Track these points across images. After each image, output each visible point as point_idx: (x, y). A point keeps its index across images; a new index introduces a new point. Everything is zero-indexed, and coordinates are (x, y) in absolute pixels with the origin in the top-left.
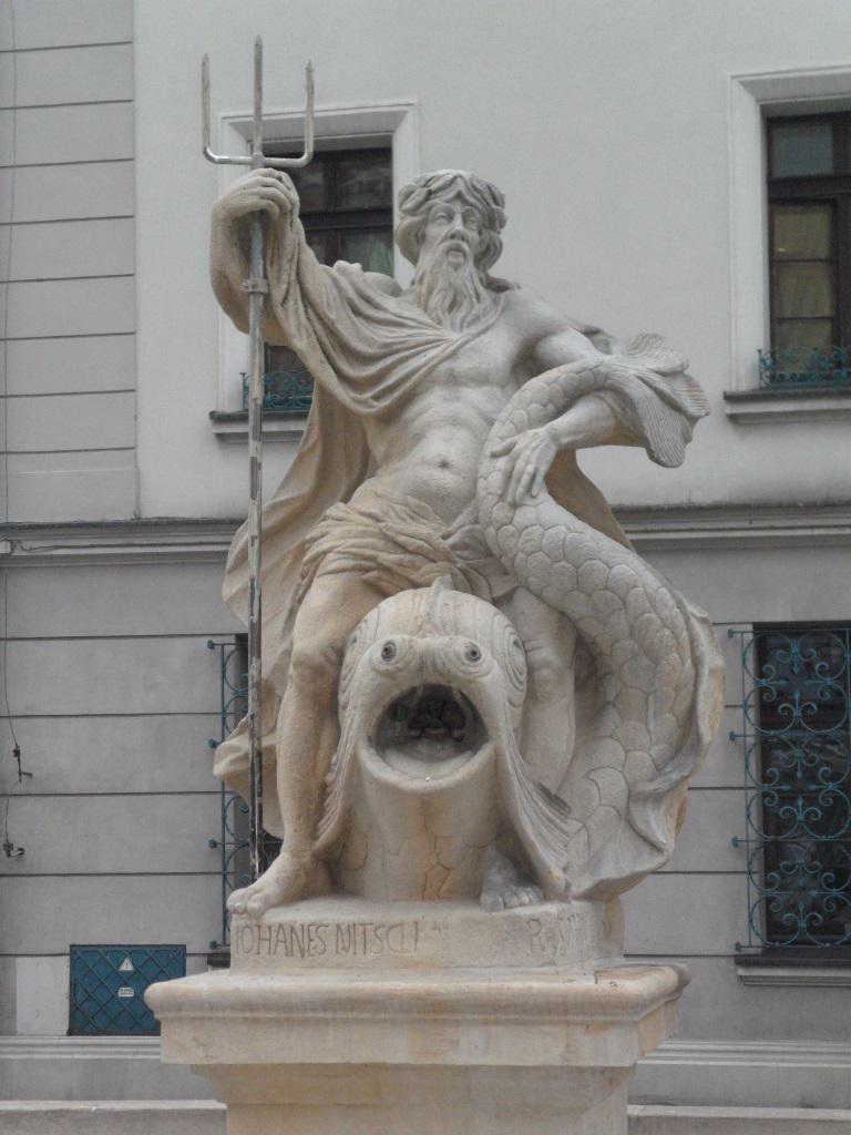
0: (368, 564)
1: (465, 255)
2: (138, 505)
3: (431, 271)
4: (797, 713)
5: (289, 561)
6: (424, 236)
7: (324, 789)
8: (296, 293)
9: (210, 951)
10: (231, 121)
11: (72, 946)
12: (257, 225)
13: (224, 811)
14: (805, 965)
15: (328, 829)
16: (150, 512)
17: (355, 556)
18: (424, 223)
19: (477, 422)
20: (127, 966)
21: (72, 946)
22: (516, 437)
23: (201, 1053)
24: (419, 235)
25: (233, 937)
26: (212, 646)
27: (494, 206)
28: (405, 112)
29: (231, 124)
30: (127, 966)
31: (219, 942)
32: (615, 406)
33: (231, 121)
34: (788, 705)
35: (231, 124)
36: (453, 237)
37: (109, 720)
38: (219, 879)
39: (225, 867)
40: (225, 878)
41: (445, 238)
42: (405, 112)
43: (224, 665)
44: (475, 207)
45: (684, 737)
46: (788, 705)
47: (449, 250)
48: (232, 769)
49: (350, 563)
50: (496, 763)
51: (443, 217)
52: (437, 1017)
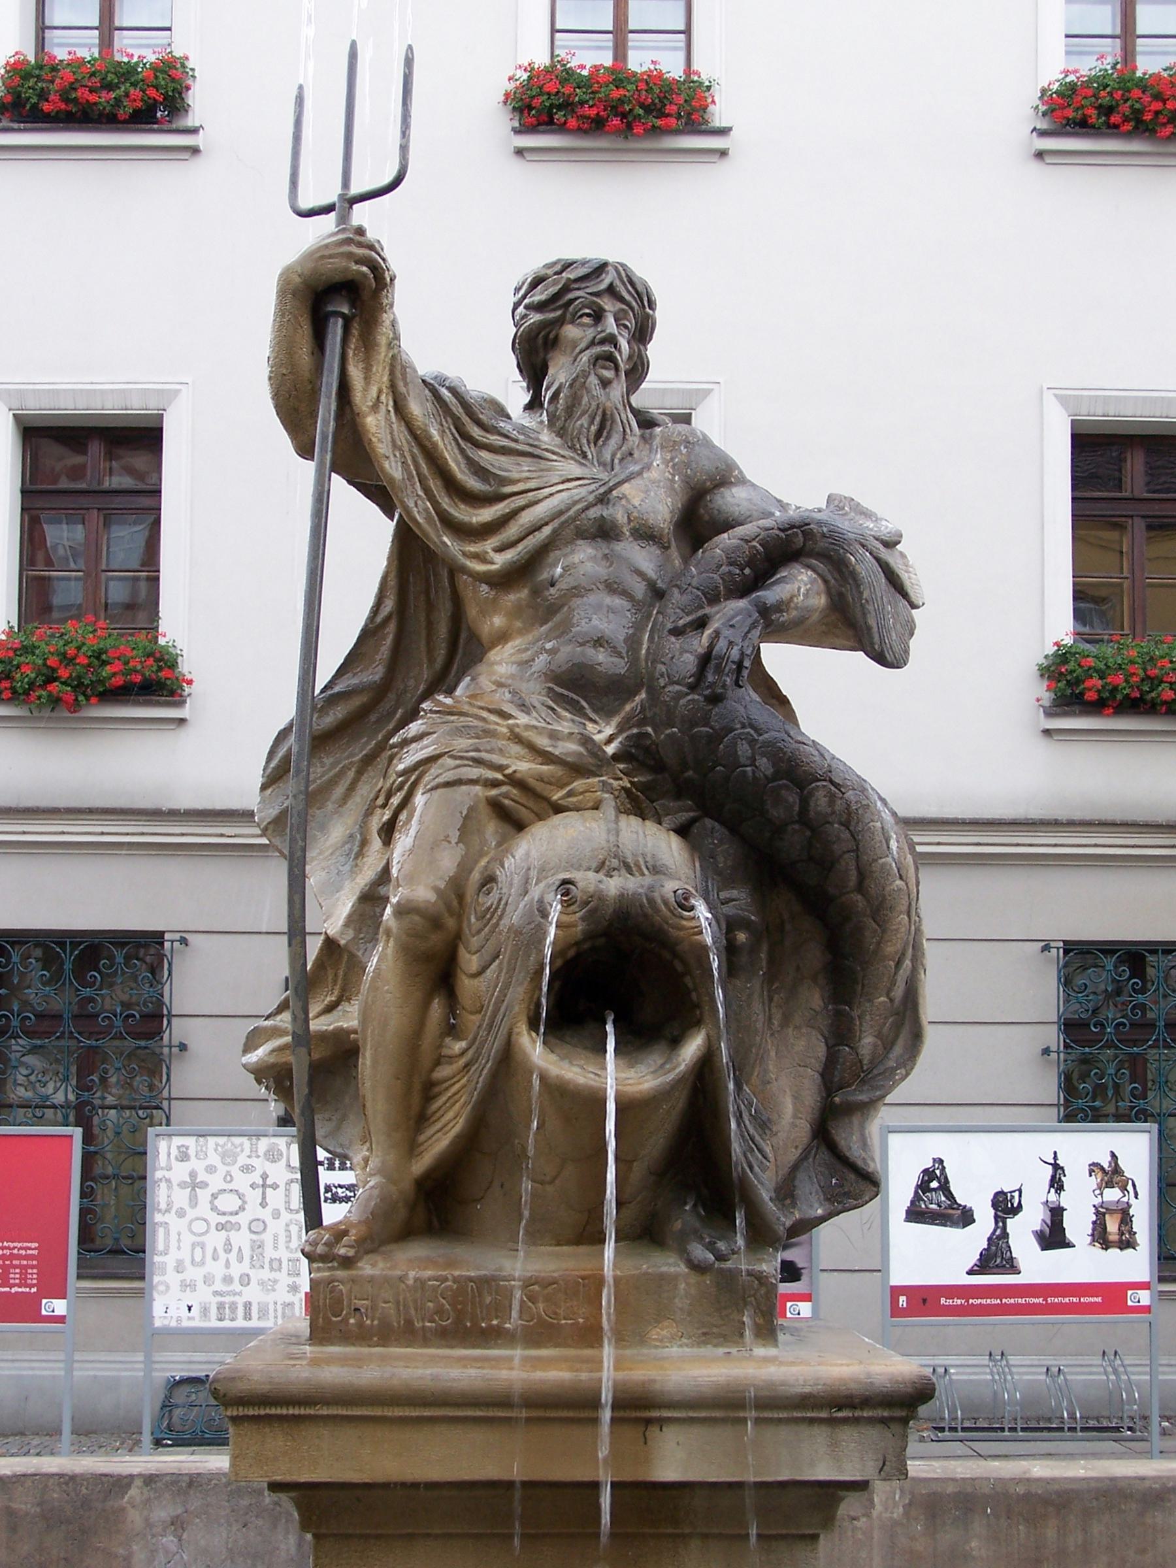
1: (617, 369)
3: (571, 386)
4: (15, 1023)
5: (351, 774)
6: (556, 338)
7: (430, 1090)
8: (387, 401)
10: (1057, 392)
14: (474, 1347)
15: (439, 1141)
18: (560, 322)
19: (639, 589)
22: (707, 610)
24: (551, 336)
25: (793, 1155)
27: (647, 310)
28: (178, 391)
29: (1056, 396)
32: (829, 577)
33: (1057, 392)
34: (98, 984)
36: (603, 342)
41: (592, 343)
42: (178, 391)
44: (632, 309)
46: (98, 984)
47: (597, 358)
48: (272, 1060)
51: (588, 315)
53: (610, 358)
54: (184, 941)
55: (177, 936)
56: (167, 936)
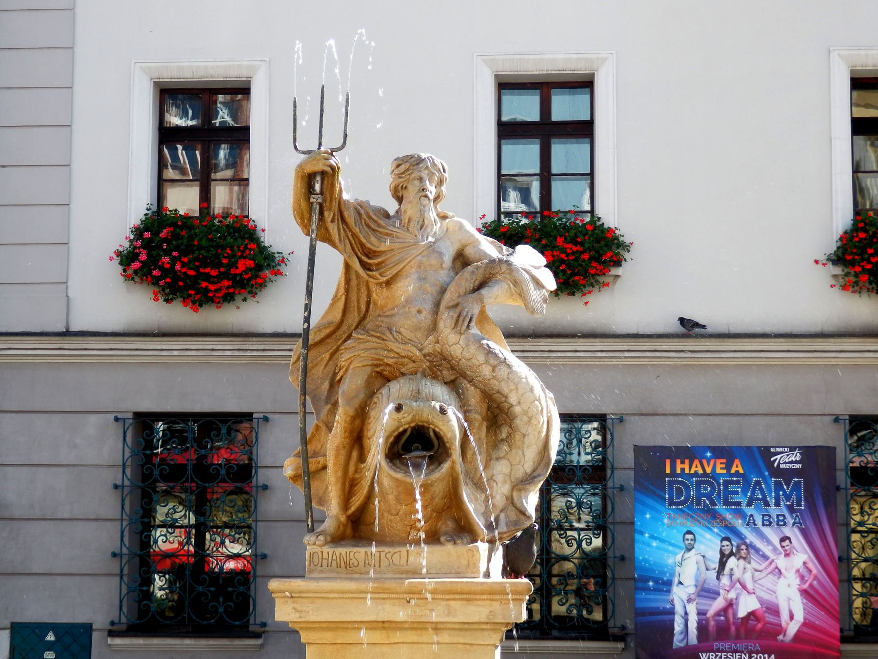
0: (378, 362)
2: (67, 323)
9: (110, 627)
11: (12, 623)
12: (318, 178)
13: (122, 532)
15: (357, 502)
16: (74, 328)
17: (373, 359)
20: (51, 637)
21: (12, 623)
23: (298, 615)
26: (117, 419)
30: (51, 637)
31: (117, 620)
35: (141, 68)
37: (42, 469)
38: (118, 579)
39: (122, 571)
40: (121, 578)
43: (125, 433)
45: (542, 459)
49: (371, 363)
50: (453, 468)
52: (657, 491)
53: (426, 196)
54: (266, 419)
55: (261, 416)
56: (255, 416)
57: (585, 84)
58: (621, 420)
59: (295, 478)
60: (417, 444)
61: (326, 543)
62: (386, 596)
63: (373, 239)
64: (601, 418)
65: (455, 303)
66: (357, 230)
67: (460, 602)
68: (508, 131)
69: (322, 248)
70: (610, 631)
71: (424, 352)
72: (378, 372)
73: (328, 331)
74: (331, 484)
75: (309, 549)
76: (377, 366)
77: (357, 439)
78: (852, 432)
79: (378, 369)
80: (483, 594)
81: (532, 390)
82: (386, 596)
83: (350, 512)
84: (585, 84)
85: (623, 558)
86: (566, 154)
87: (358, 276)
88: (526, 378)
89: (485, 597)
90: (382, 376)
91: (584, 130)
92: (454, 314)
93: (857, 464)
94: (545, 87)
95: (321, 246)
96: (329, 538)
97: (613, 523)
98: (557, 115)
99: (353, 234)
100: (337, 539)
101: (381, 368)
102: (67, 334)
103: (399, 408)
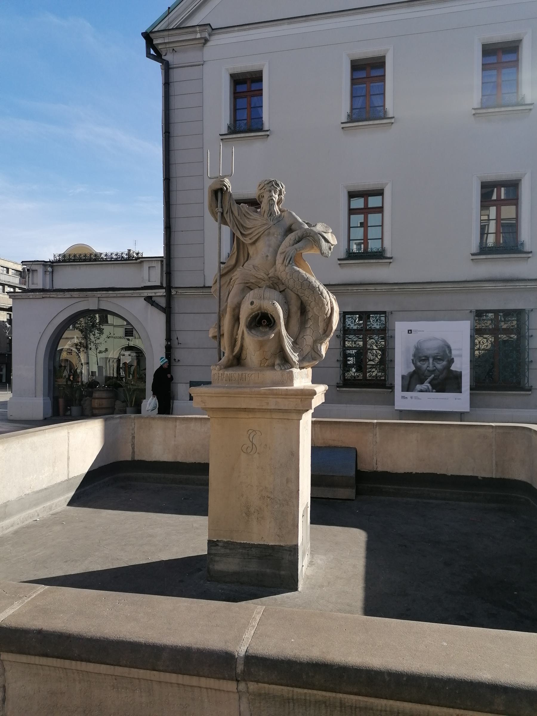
16: (206, 285)
53: (272, 199)
57: (380, 193)
58: (392, 313)
59: (214, 337)
60: (263, 321)
61: (220, 369)
62: (245, 396)
63: (247, 222)
64: (384, 312)
65: (283, 251)
66: (239, 218)
67: (281, 399)
68: (352, 212)
69: (224, 227)
70: (387, 385)
71: (269, 276)
72: (248, 287)
73: (229, 269)
74: (225, 342)
75: (213, 372)
76: (247, 283)
77: (236, 319)
78: (477, 316)
79: (247, 285)
80: (292, 395)
81: (322, 294)
82: (245, 396)
83: (234, 354)
84: (380, 193)
85: (391, 361)
86: (373, 219)
87: (238, 239)
88: (318, 287)
89: (293, 397)
90: (248, 287)
91: (380, 210)
92: (282, 256)
93: (478, 327)
94: (365, 194)
95: (223, 226)
96: (222, 367)
97: (388, 349)
98: (370, 205)
99: (238, 220)
100: (229, 366)
101: (249, 284)
102: (204, 287)
103: (252, 303)
